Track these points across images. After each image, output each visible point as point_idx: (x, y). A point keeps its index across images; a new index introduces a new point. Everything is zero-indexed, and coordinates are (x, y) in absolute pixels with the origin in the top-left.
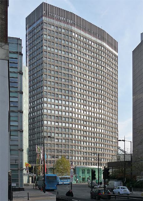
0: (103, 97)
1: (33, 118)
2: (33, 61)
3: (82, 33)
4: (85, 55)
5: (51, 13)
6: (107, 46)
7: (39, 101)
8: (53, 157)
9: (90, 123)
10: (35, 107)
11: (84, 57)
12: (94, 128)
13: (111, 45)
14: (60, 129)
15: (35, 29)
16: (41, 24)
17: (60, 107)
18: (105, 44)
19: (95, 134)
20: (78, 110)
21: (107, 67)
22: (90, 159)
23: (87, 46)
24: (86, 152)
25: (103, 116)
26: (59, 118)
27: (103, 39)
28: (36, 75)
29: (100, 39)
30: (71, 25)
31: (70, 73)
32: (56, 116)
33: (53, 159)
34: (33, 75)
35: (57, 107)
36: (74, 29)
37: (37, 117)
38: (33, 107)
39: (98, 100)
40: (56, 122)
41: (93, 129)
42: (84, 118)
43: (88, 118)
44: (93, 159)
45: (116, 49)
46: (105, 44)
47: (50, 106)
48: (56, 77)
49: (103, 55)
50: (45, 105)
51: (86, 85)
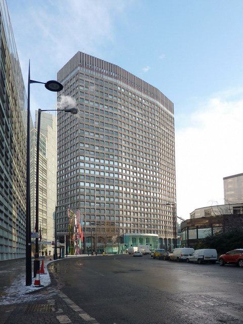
0: (158, 174)
1: (66, 181)
2: (65, 123)
3: (130, 88)
4: (134, 135)
5: (89, 63)
6: (162, 106)
7: (74, 167)
8: (93, 224)
9: (142, 203)
10: (68, 167)
11: (133, 114)
12: (147, 192)
13: (166, 106)
14: (102, 192)
15: (68, 83)
16: (76, 75)
17: (102, 168)
18: (158, 103)
19: (149, 215)
20: (125, 171)
21: (161, 127)
22: (143, 226)
23: (137, 103)
24: (137, 219)
25: (158, 179)
26: (99, 180)
27: (157, 98)
28: (69, 169)
29: (154, 98)
30: (116, 78)
31: (115, 130)
32: (97, 222)
33: (93, 226)
34: (66, 193)
35: (98, 198)
36: (118, 82)
37: (71, 179)
38: (66, 169)
39: (151, 162)
40: (97, 159)
41: (146, 193)
42: (133, 180)
43: (138, 181)
44: (146, 227)
45: (172, 110)
46: (158, 103)
47: (87, 165)
48: (96, 134)
49: (156, 124)
50: (82, 164)
51: (136, 161)
